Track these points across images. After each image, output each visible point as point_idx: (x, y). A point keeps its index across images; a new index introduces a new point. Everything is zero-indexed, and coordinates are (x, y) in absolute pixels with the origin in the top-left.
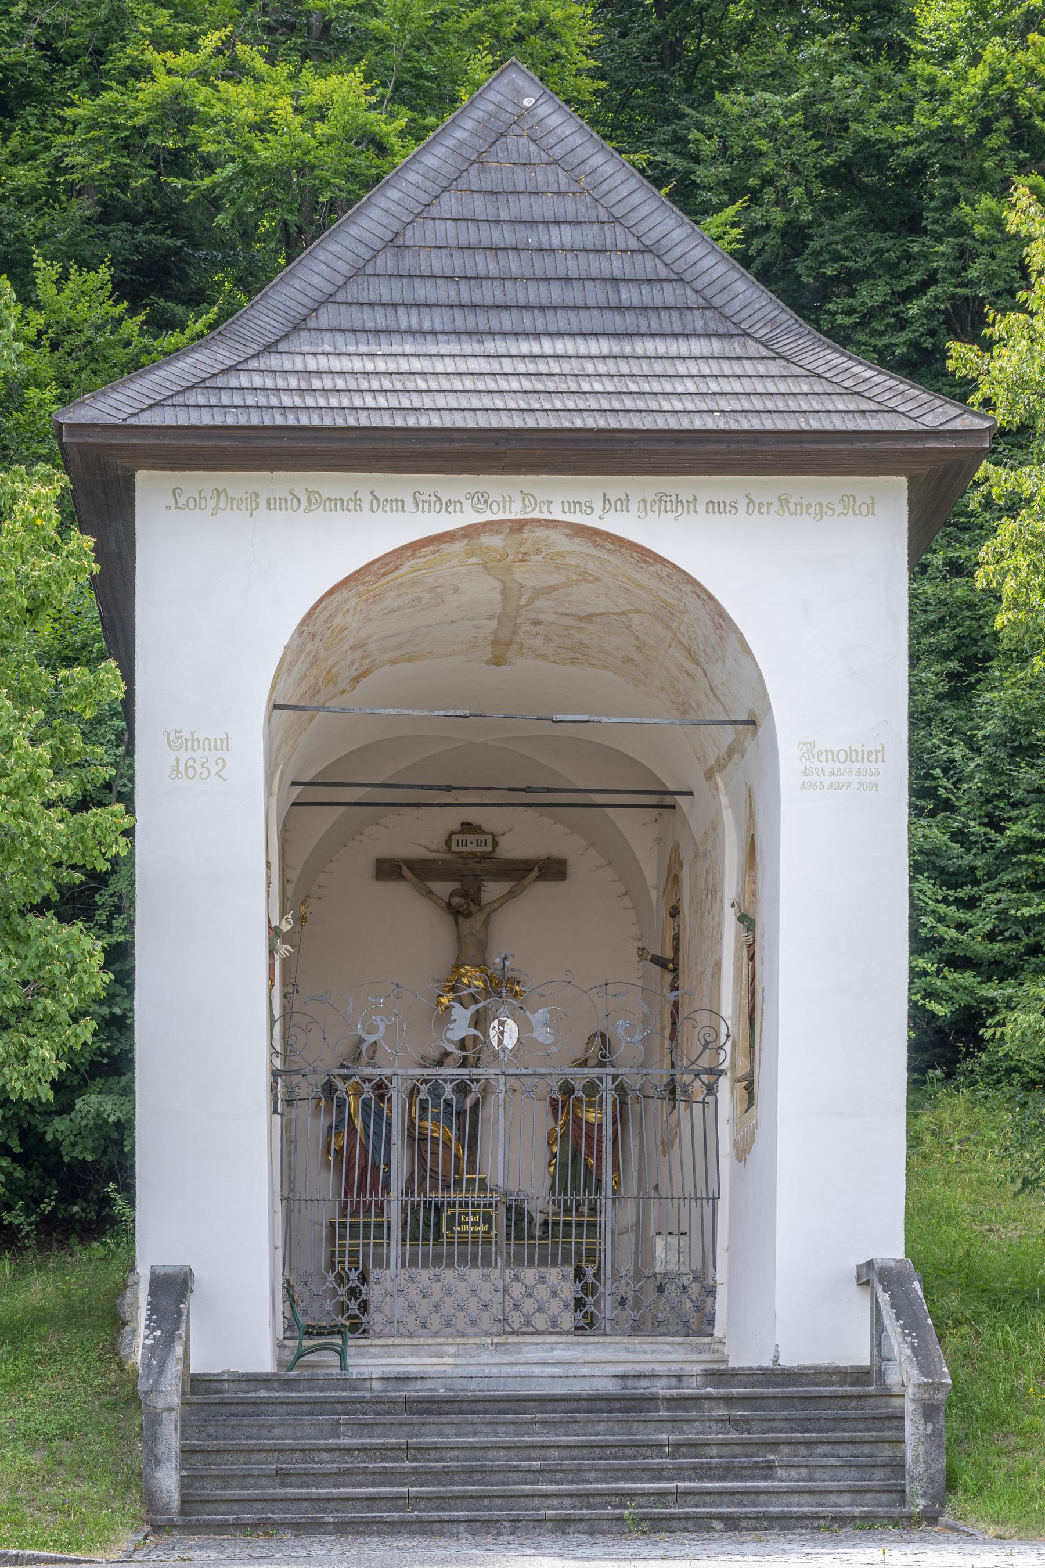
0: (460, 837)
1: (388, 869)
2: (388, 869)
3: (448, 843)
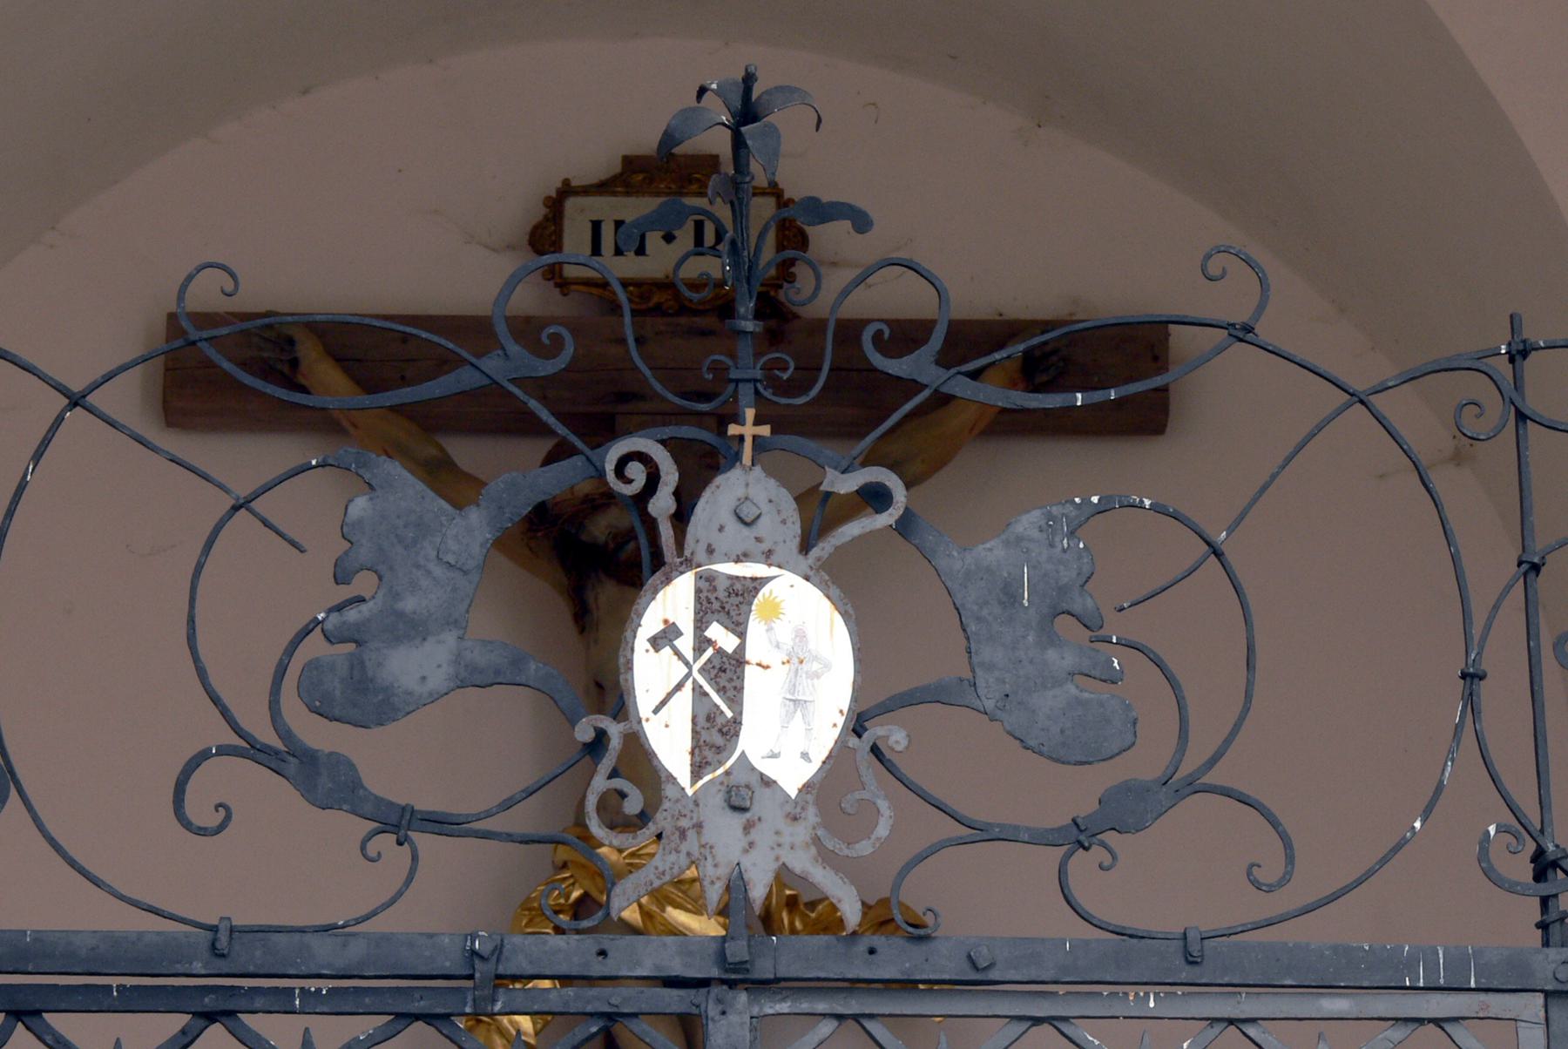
0: (610, 208)
1: (233, 371)
2: (233, 371)
3: (545, 235)
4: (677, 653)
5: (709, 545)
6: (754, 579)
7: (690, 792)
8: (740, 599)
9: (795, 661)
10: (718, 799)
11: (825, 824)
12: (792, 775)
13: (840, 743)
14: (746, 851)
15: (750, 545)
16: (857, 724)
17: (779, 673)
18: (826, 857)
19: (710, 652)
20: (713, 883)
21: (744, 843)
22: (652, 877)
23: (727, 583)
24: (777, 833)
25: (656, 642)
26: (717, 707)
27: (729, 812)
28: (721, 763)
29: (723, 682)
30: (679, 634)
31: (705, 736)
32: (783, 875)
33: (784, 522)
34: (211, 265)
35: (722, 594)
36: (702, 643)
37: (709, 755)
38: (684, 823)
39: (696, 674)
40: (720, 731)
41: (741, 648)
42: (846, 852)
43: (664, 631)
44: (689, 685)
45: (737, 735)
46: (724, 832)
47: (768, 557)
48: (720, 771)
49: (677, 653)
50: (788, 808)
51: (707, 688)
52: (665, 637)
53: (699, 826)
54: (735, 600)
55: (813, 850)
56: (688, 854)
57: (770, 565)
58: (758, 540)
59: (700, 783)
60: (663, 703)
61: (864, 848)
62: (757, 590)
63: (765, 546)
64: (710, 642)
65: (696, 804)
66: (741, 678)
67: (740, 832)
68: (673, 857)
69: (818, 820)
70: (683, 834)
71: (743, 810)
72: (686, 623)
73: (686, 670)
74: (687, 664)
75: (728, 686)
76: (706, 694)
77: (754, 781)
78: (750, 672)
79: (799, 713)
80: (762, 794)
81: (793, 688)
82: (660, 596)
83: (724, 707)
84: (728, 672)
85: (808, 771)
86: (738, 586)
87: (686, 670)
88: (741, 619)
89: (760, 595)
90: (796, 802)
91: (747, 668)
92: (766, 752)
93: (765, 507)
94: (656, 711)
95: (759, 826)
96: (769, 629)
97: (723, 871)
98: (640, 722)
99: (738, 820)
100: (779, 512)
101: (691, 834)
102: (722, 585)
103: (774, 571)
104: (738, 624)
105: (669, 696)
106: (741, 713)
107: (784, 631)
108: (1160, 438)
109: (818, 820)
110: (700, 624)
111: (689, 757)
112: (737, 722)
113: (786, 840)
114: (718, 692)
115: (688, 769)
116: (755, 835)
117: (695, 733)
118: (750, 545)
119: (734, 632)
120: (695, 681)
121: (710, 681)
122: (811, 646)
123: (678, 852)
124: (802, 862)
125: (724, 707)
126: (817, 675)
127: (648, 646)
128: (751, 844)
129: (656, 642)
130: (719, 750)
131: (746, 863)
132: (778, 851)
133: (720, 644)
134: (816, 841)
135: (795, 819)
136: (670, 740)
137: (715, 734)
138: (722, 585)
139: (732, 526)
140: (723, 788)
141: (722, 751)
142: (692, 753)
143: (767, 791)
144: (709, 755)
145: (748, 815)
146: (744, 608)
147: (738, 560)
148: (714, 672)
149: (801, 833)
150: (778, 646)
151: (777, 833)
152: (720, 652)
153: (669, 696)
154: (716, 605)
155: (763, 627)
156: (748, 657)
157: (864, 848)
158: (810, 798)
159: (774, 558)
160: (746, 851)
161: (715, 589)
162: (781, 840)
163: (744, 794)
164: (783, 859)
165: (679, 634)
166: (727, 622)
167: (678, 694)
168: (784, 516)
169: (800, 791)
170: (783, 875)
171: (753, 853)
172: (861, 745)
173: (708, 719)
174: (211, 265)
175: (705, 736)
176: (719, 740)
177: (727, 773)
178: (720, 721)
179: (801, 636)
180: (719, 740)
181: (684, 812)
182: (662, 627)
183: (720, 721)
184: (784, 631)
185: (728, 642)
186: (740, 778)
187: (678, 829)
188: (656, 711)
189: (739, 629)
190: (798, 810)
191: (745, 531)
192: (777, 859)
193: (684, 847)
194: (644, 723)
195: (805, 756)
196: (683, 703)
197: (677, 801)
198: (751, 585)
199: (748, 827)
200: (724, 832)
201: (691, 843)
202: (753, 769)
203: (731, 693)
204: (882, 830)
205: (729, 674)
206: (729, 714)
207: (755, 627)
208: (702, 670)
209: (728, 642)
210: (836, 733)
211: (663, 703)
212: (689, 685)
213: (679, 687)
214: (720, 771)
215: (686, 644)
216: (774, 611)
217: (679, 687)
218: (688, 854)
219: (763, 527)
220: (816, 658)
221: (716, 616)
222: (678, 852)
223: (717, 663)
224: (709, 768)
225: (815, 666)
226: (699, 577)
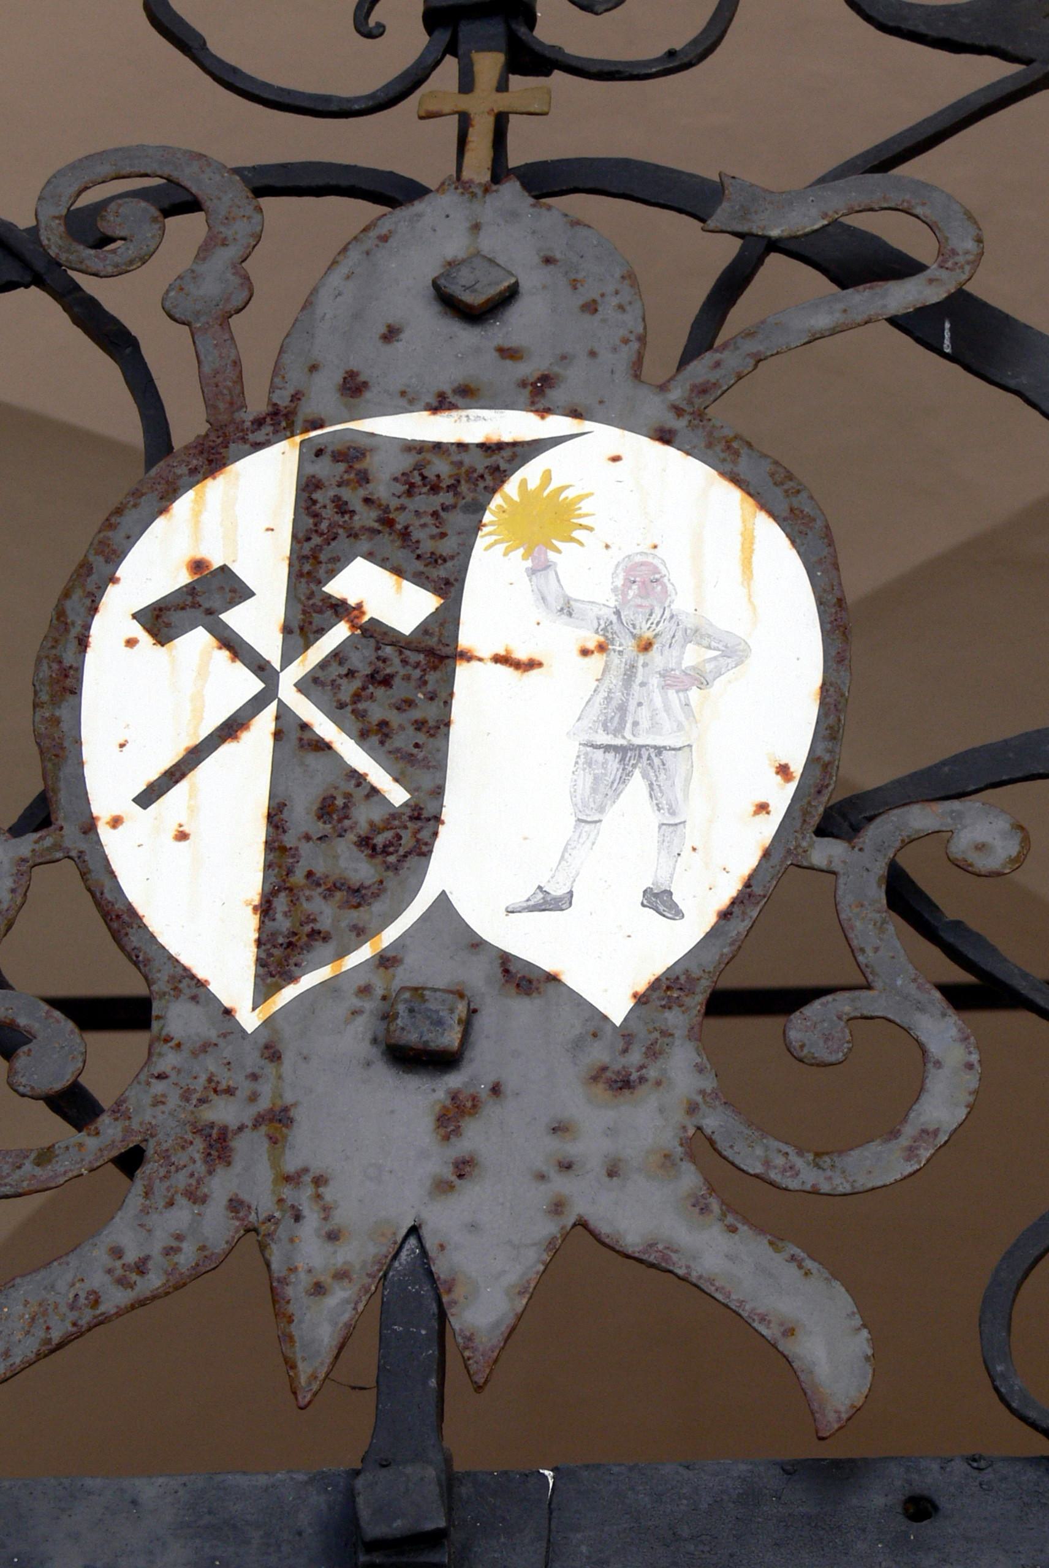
4: (234, 646)
5: (351, 375)
6: (489, 448)
7: (249, 1020)
8: (447, 498)
9: (629, 645)
10: (355, 1039)
11: (727, 1096)
12: (612, 957)
13: (781, 864)
14: (443, 1187)
15: (484, 367)
16: (829, 809)
17: (570, 685)
18: (733, 1194)
19: (339, 633)
20: (319, 1289)
21: (438, 1164)
22: (98, 1280)
23: (407, 462)
24: (559, 1129)
25: (161, 621)
26: (358, 778)
27: (385, 1075)
28: (362, 933)
29: (376, 712)
30: (239, 592)
31: (311, 859)
32: (580, 1246)
33: (591, 307)
34: (675, 63)
35: (383, 489)
36: (309, 612)
37: (326, 912)
38: (224, 1112)
39: (287, 692)
40: (365, 842)
41: (446, 620)
42: (808, 1176)
43: (190, 590)
44: (265, 722)
45: (423, 850)
46: (373, 1150)
47: (538, 394)
48: (363, 954)
49: (234, 646)
50: (599, 1054)
51: (325, 728)
52: (204, 598)
53: (278, 1121)
54: (425, 502)
55: (690, 1179)
56: (236, 1205)
57: (544, 412)
58: (508, 353)
59: (289, 993)
60: (174, 775)
61: (881, 1164)
62: (500, 476)
63: (528, 369)
64: (339, 609)
65: (272, 1053)
66: (443, 697)
67: (426, 1123)
68: (181, 1216)
69: (709, 1083)
70: (219, 1145)
71: (441, 1061)
72: (264, 563)
73: (255, 685)
74: (260, 667)
75: (395, 718)
76: (323, 747)
77: (477, 976)
78: (473, 688)
79: (637, 784)
80: (505, 1020)
81: (618, 715)
82: (183, 504)
83: (379, 777)
84: (403, 689)
85: (670, 944)
86: (441, 467)
87: (255, 685)
88: (446, 547)
89: (511, 487)
90: (626, 1035)
91: (463, 672)
92: (523, 892)
93: (530, 279)
94: (148, 797)
95: (492, 1111)
96: (480, 660)
97: (359, 1253)
98: (90, 826)
99: (419, 1097)
100: (574, 284)
101: (250, 1149)
102: (385, 473)
103: (557, 425)
104: (436, 560)
105: (195, 756)
106: (439, 792)
107: (587, 571)
108: (470, 95)
109: (709, 1083)
110: (311, 561)
111: (252, 922)
112: (421, 823)
113: (592, 1147)
114: (361, 737)
115: (250, 953)
116: (475, 1137)
117: (278, 851)
118: (484, 367)
119: (420, 580)
120: (284, 713)
121: (336, 711)
122: (682, 603)
123: (196, 1197)
124: (646, 1213)
125: (379, 777)
126: (700, 679)
127: (137, 630)
128: (464, 1168)
129: (161, 621)
130: (357, 896)
131: (443, 1221)
132: (561, 1184)
133: (373, 611)
134: (701, 1147)
135: (623, 1084)
136: (193, 882)
137: (340, 855)
138: (385, 473)
139: (426, 323)
140: (370, 1005)
141: (364, 902)
142: (265, 909)
143: (523, 1008)
144: (326, 912)
145: (454, 1080)
146: (456, 520)
147: (440, 404)
148: (348, 688)
149: (648, 1124)
150: (567, 609)
151: (559, 1129)
152: (374, 633)
153: (195, 756)
154: (366, 517)
155: (518, 563)
156: (466, 639)
157: (881, 1164)
158: (676, 1020)
159: (555, 395)
160: (443, 1187)
161: (364, 478)
162: (572, 1149)
163: (442, 1027)
164: (580, 1208)
165: (239, 592)
166: (400, 555)
167: (226, 750)
168: (590, 292)
169: (641, 1000)
170: (580, 1246)
171: (472, 1196)
172: (855, 866)
173: (326, 809)
174: (675, 63)
175: (311, 859)
176: (361, 870)
177: (385, 961)
178: (364, 815)
179: (644, 579)
180: (361, 870)
181: (225, 1079)
182: (184, 578)
183: (364, 815)
184: (587, 571)
185: (404, 606)
186: (431, 970)
187: (202, 1130)
188: (148, 797)
189: (441, 572)
190: (636, 1057)
191: (467, 336)
192: (558, 1207)
193: (221, 1186)
194: (104, 832)
195: (660, 901)
196: (244, 775)
197: (206, 1047)
198: (481, 463)
199: (452, 1118)
200: (373, 1150)
201: (250, 1175)
202: (477, 944)
203: (403, 740)
204: (942, 1107)
205: (400, 690)
206: (397, 795)
207: (493, 571)
208: (308, 685)
209: (404, 606)
210: (768, 828)
211: (174, 775)
212: (265, 722)
213: (231, 729)
214: (363, 954)
215: (260, 621)
216: (557, 520)
217: (231, 729)
218: (236, 1205)
219: (519, 324)
220: (696, 635)
221: (365, 545)
222: (196, 1197)
223: (361, 662)
224: (322, 949)
225: (692, 656)
226: (313, 453)
